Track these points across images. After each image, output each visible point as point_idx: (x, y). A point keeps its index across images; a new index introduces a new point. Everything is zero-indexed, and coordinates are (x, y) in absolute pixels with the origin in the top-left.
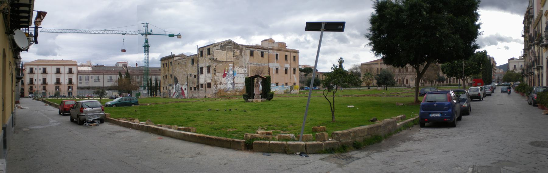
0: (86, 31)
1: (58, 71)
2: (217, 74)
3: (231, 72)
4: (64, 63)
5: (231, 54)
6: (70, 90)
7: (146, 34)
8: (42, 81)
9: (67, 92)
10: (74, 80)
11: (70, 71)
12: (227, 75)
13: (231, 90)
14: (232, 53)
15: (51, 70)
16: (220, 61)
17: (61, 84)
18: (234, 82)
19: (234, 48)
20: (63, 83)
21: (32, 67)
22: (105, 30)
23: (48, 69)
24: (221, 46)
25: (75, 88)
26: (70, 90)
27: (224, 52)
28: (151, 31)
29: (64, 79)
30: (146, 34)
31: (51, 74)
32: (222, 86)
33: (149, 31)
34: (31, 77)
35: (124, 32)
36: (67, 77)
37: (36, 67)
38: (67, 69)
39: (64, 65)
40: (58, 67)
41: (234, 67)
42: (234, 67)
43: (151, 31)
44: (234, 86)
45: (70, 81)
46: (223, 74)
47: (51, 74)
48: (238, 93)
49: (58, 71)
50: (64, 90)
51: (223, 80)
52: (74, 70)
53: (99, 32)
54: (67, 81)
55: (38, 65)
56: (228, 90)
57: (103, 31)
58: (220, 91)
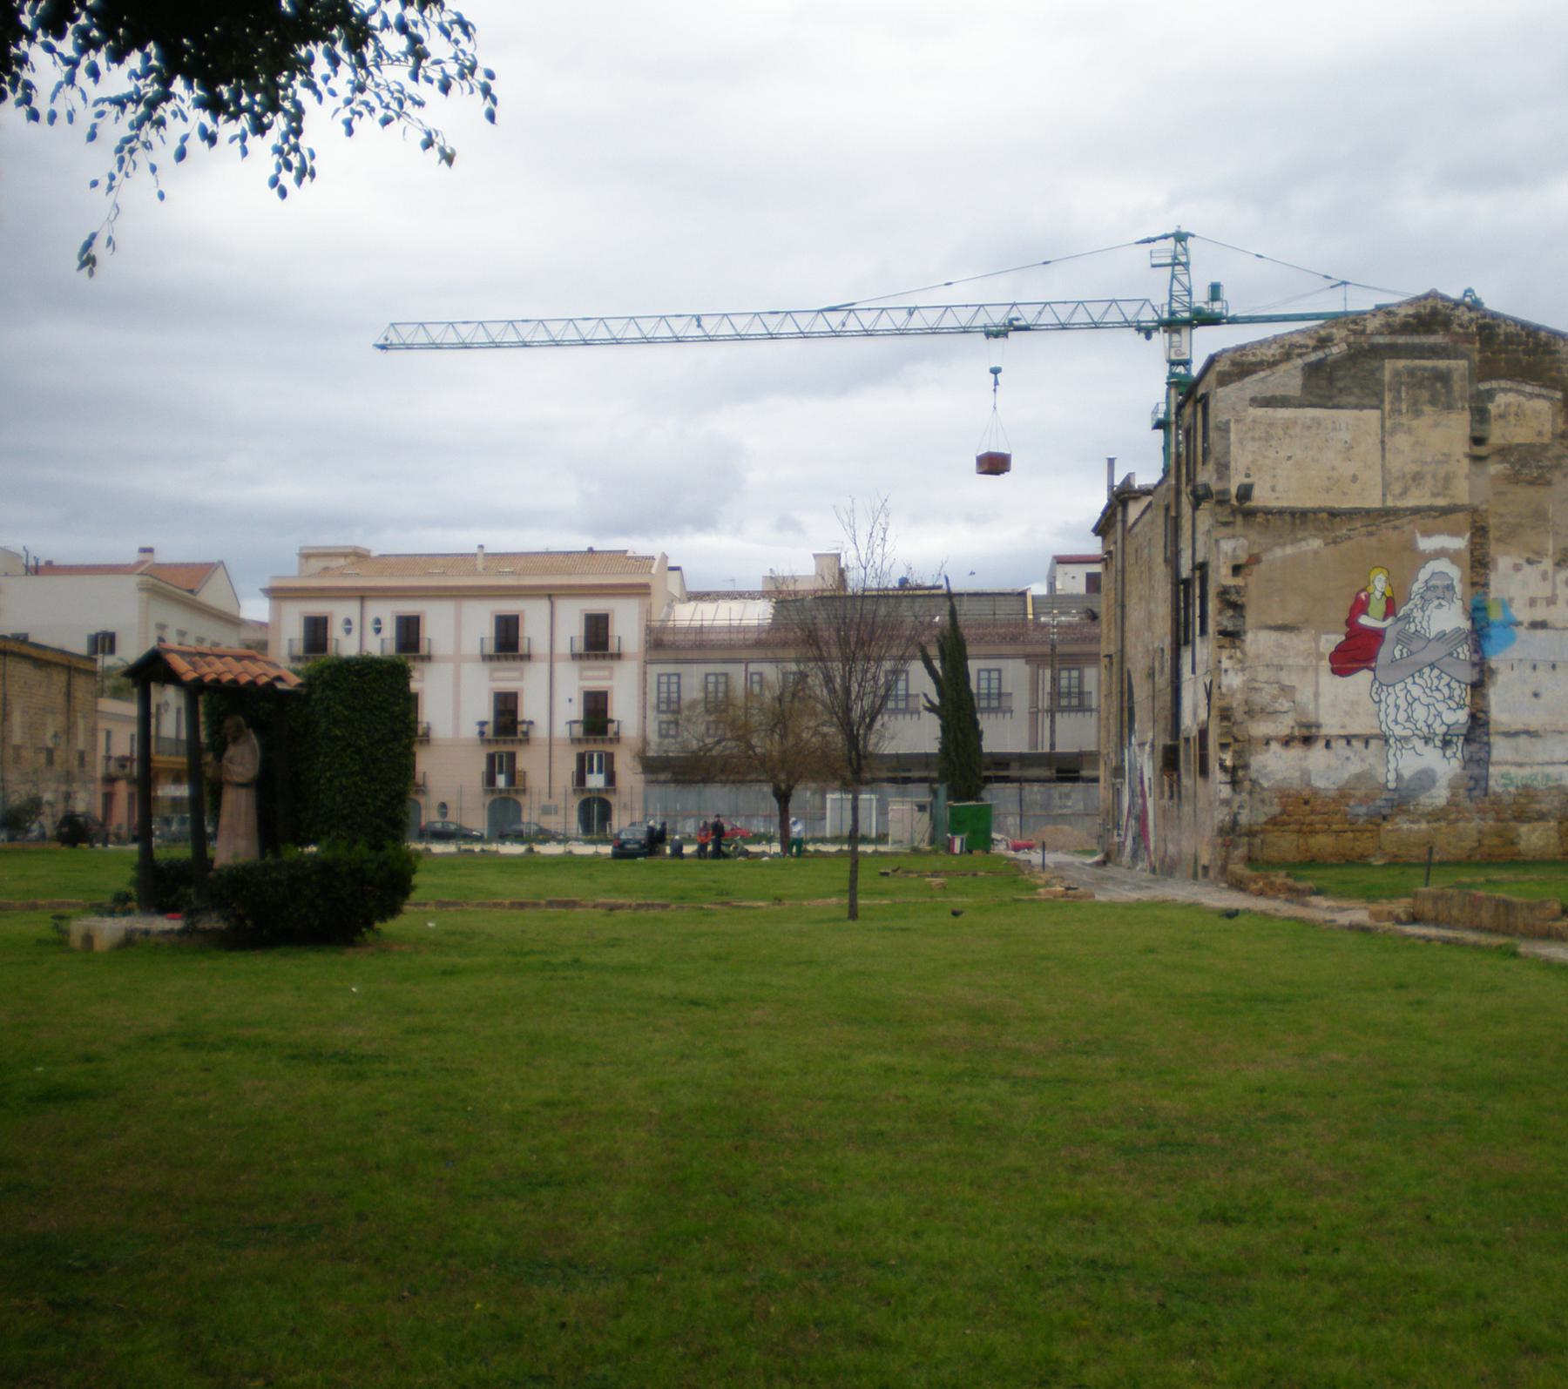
0: (710, 326)
1: (507, 641)
2: (1258, 641)
3: (1449, 618)
4: (550, 578)
5: (1447, 433)
6: (596, 781)
7: (1172, 325)
8: (576, 711)
9: (575, 802)
10: (625, 711)
11: (597, 639)
12: (1388, 651)
13: (1439, 796)
14: (1459, 425)
15: (552, 628)
16: (1299, 517)
17: (526, 740)
18: (1478, 723)
19: (1485, 371)
20: (540, 732)
21: (317, 608)
22: (848, 308)
23: (534, 622)
24: (1313, 370)
25: (625, 766)
26: (596, 781)
27: (1352, 425)
28: (1215, 291)
29: (551, 699)
30: (1172, 325)
31: (458, 659)
32: (1317, 758)
33: (1200, 298)
34: (596, 685)
35: (998, 317)
36: (572, 684)
37: (350, 609)
38: (571, 621)
39: (550, 594)
40: (508, 607)
41: (1479, 564)
42: (1479, 564)
43: (1215, 291)
44: (1478, 763)
45: (596, 714)
46: (1331, 641)
47: (458, 659)
48: (1534, 837)
49: (507, 641)
50: (548, 769)
51: (1341, 700)
52: (627, 627)
53: (804, 322)
54: (571, 710)
55: (363, 595)
56: (1401, 800)
57: (835, 319)
58: (1300, 808)
